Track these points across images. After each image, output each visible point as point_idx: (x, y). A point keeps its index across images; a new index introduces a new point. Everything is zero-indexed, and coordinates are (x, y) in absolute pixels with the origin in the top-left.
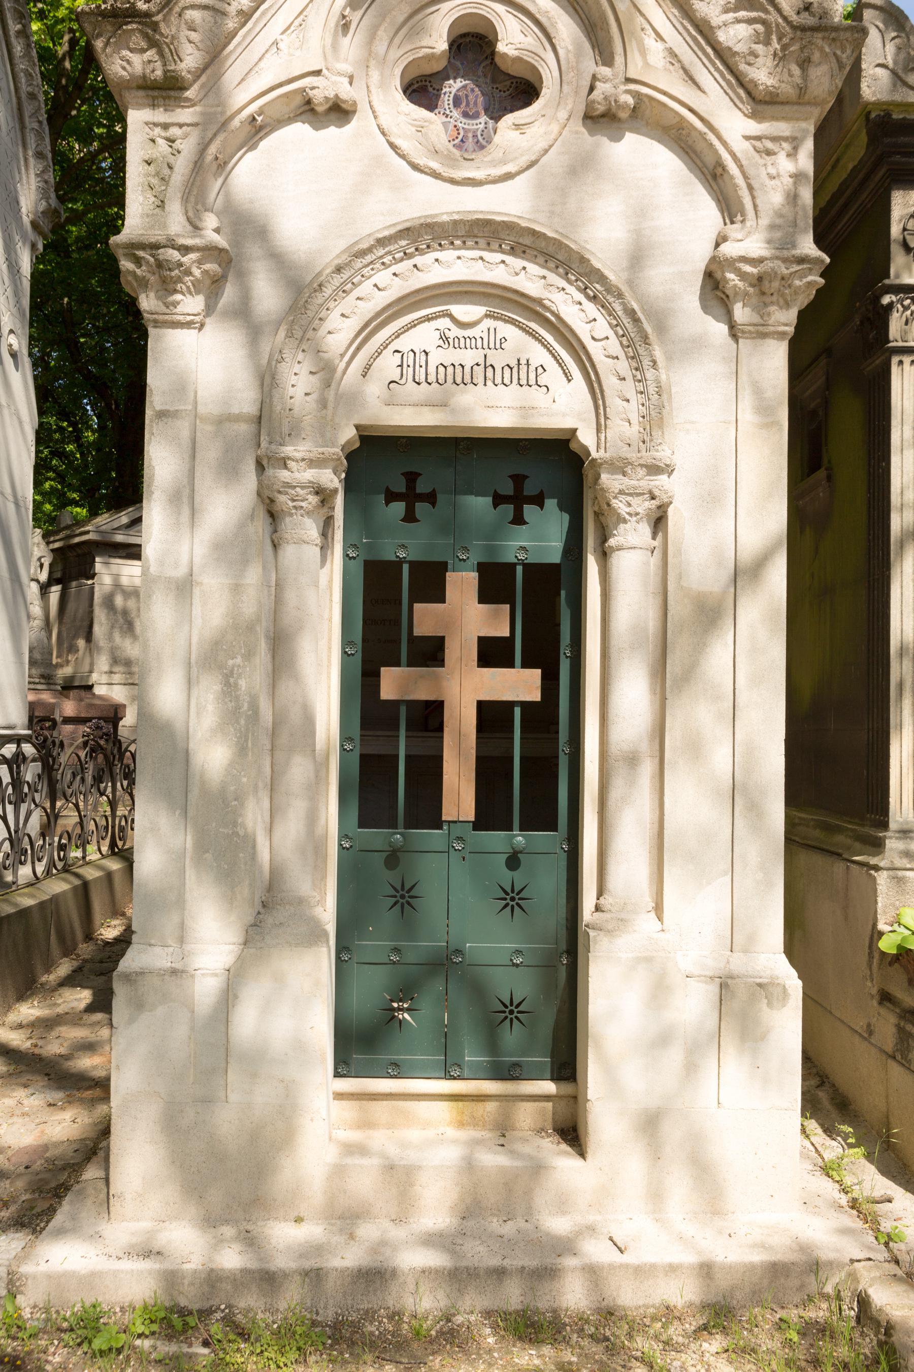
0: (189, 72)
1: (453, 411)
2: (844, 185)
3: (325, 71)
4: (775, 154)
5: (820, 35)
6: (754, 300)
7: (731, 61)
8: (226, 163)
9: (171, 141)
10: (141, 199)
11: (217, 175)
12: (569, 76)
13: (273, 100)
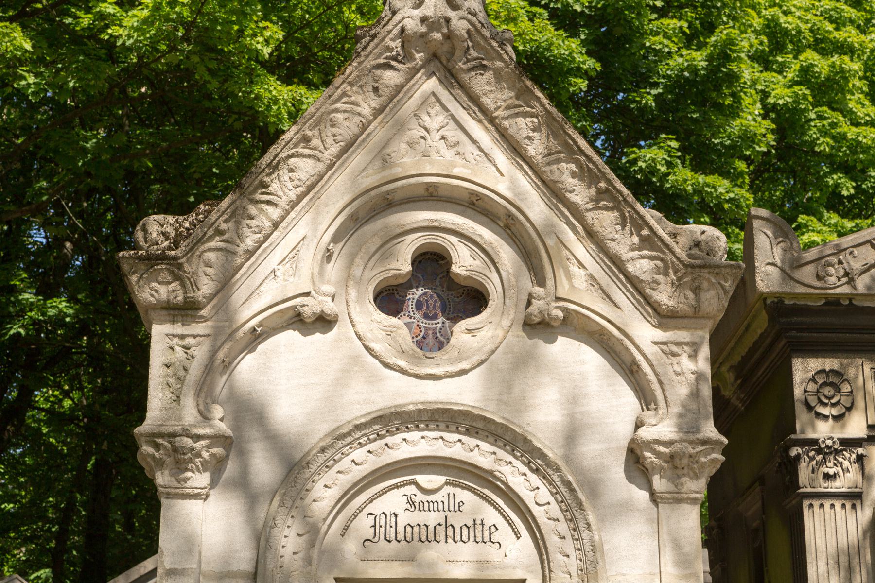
0: (204, 297)
1: (420, 565)
2: (752, 351)
3: (313, 293)
4: (679, 355)
5: (706, 271)
6: (669, 473)
7: (639, 286)
8: (230, 364)
9: (186, 348)
10: (161, 395)
11: (222, 373)
12: (511, 293)
13: (270, 316)
